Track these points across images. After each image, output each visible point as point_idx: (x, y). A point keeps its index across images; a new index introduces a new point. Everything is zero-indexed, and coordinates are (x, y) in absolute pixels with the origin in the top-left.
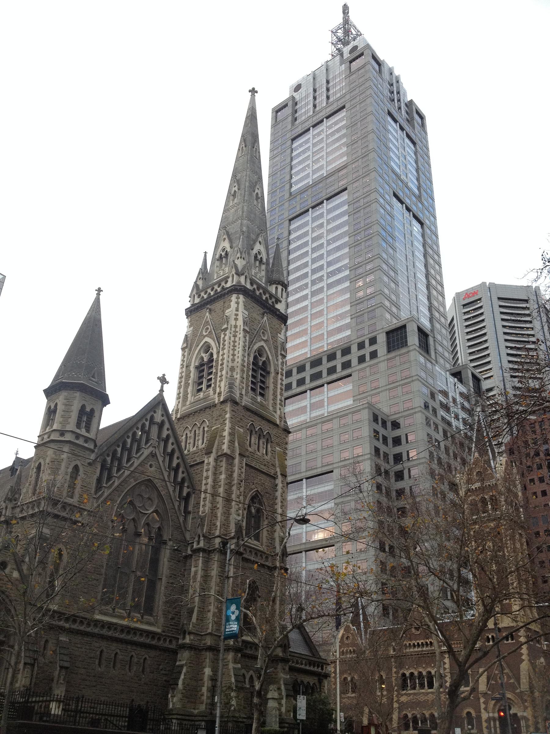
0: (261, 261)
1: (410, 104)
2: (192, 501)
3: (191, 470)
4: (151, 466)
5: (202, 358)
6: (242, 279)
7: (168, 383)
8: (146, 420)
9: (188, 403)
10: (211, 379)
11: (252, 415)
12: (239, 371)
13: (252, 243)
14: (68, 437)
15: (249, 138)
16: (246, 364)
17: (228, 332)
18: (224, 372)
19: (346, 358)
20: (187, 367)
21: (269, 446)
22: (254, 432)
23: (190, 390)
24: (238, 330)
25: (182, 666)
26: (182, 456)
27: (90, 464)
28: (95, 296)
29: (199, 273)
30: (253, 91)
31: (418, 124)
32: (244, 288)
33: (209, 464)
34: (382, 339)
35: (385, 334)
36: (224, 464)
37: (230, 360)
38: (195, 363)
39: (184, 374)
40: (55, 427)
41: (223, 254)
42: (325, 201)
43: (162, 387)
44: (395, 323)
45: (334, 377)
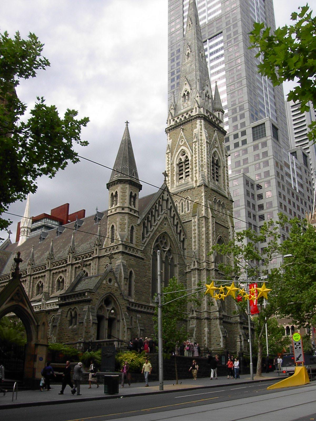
2: (186, 243)
3: (183, 225)
4: (165, 224)
5: (181, 159)
9: (175, 186)
11: (215, 193)
12: (206, 167)
14: (126, 211)
17: (197, 144)
18: (197, 168)
20: (171, 164)
21: (224, 210)
22: (216, 203)
24: (203, 142)
25: (193, 330)
27: (138, 225)
28: (125, 126)
34: (249, 132)
36: (204, 222)
37: (200, 161)
38: (176, 162)
40: (118, 205)
41: (186, 93)
42: (208, 40)
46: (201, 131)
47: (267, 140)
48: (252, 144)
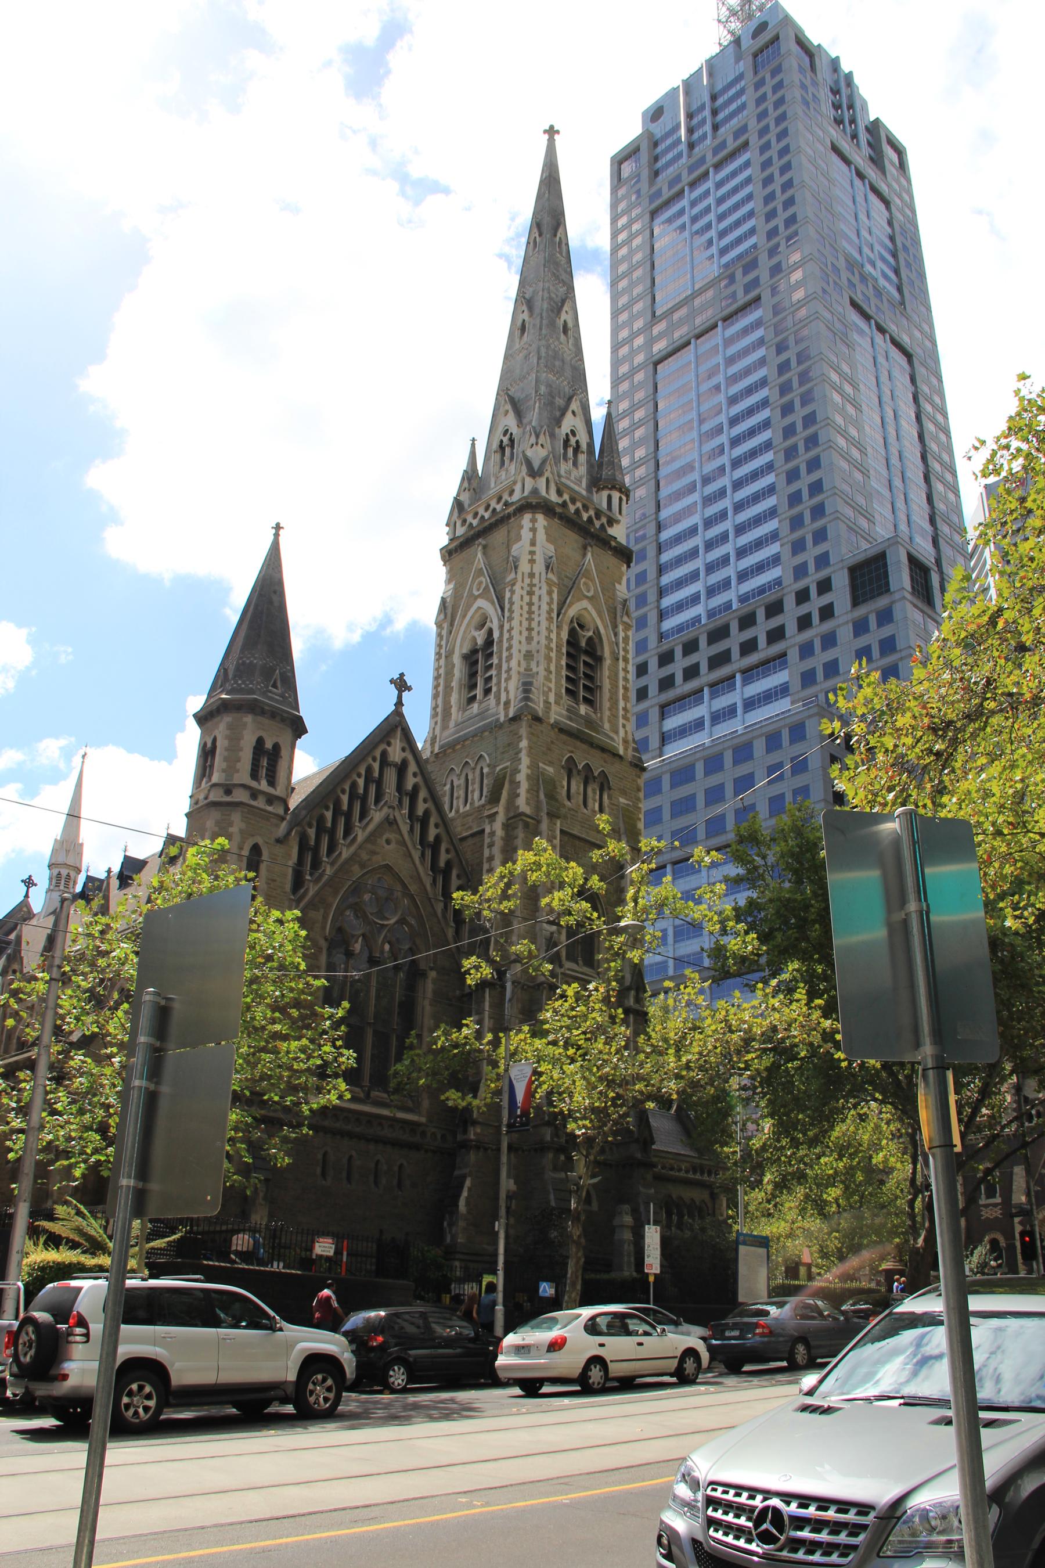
0: (577, 449)
1: (875, 128)
4: (388, 842)
5: (474, 639)
6: (541, 483)
7: (409, 689)
8: (374, 759)
9: (452, 724)
10: (490, 678)
13: (558, 414)
15: (547, 220)
16: (553, 645)
17: (517, 588)
19: (775, 622)
21: (605, 797)
22: (575, 772)
23: (454, 699)
24: (536, 581)
26: (444, 822)
27: (278, 841)
28: (272, 538)
29: (463, 479)
30: (551, 132)
31: (893, 164)
32: (540, 499)
33: (493, 834)
34: (841, 581)
35: (846, 571)
37: (523, 640)
38: (461, 648)
39: (442, 671)
40: (215, 779)
41: (506, 440)
43: (400, 697)
44: (864, 549)
45: (753, 659)
46: (533, 549)
47: (893, 602)
48: (850, 616)
